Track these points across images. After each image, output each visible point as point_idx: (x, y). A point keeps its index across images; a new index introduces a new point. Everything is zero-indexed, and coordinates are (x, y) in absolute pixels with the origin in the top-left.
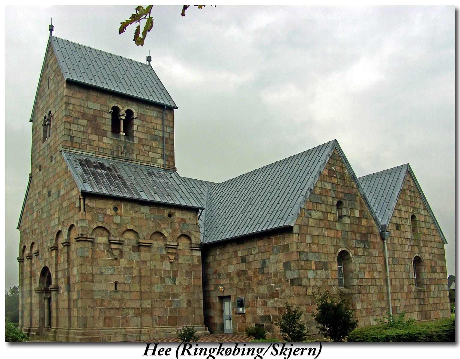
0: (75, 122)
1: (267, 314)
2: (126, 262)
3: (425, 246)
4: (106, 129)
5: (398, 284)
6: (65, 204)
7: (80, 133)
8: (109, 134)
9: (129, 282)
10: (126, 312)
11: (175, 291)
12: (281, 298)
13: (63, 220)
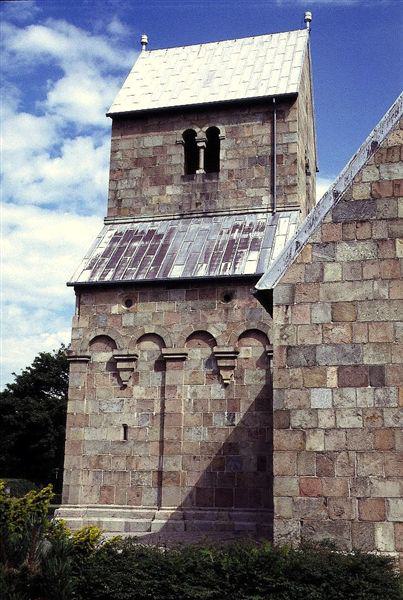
2: (143, 390)
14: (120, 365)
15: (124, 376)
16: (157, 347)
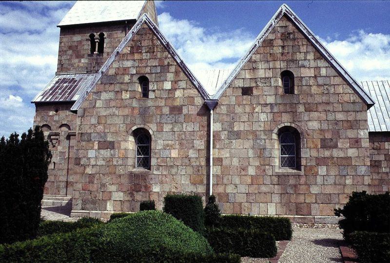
2: (62, 148)
14: (52, 137)
16: (67, 129)
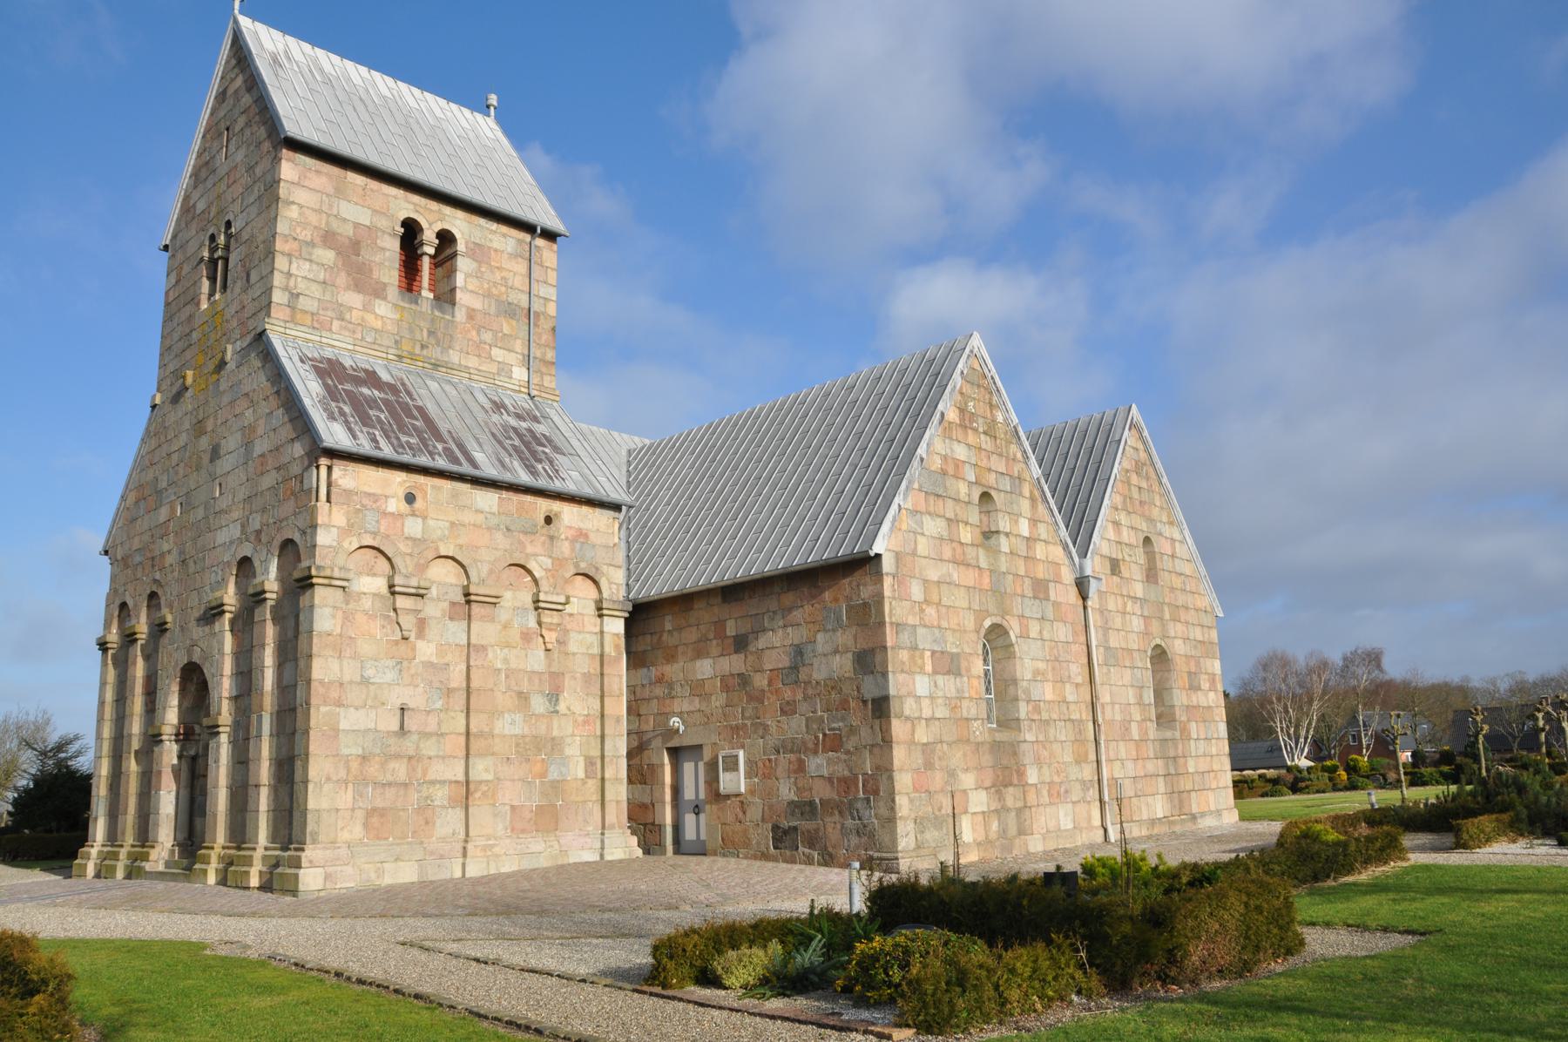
0: (304, 255)
1: (806, 796)
3: (1175, 620)
4: (385, 280)
5: (1118, 717)
6: (268, 481)
7: (314, 287)
8: (393, 292)
9: (439, 705)
10: (425, 794)
11: (555, 733)
12: (848, 752)
13: (258, 527)
15: (408, 622)
